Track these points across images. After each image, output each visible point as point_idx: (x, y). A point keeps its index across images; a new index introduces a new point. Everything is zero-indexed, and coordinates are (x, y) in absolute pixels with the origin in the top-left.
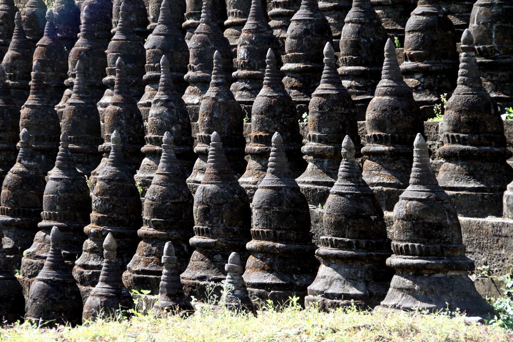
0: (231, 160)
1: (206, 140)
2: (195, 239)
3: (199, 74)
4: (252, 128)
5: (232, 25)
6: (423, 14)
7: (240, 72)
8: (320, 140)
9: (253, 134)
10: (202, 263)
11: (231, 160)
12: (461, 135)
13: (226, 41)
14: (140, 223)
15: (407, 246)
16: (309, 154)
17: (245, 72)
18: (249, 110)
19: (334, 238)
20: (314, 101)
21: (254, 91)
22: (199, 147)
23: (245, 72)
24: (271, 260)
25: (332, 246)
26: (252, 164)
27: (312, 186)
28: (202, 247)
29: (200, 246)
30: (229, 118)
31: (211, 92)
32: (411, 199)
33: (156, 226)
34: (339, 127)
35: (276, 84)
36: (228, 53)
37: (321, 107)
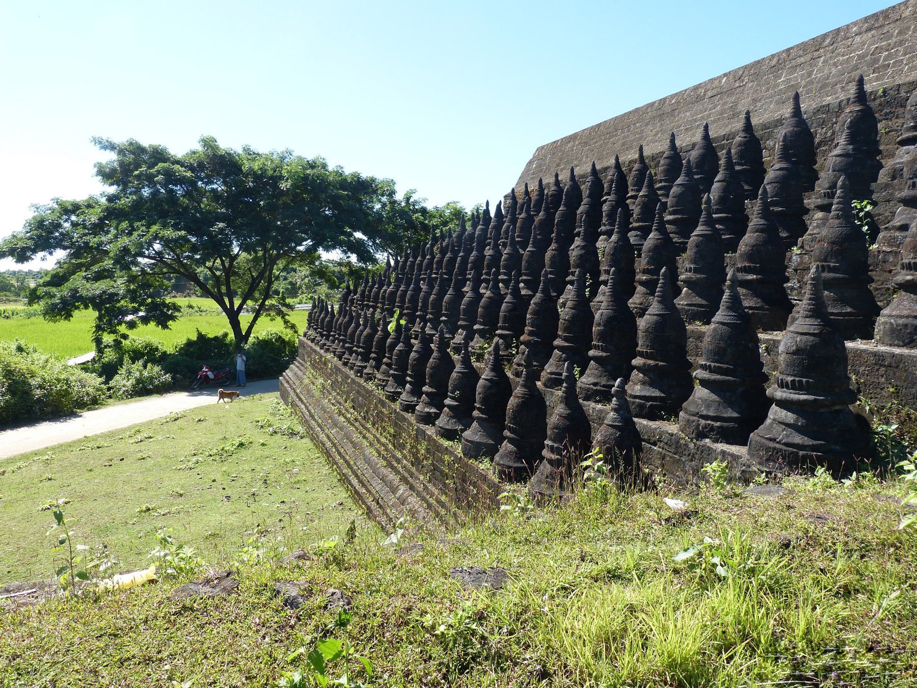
0: (623, 288)
1: (607, 272)
2: (591, 353)
3: (608, 228)
4: (642, 263)
5: (631, 197)
6: (780, 169)
7: (635, 225)
8: (696, 271)
9: (642, 267)
10: (596, 372)
11: (623, 288)
12: (832, 265)
13: (627, 205)
14: (556, 336)
15: (793, 381)
16: (684, 281)
17: (638, 224)
18: (640, 250)
19: (713, 364)
20: (693, 239)
21: (644, 236)
22: (603, 278)
23: (638, 224)
24: (653, 376)
25: (710, 372)
26: (640, 289)
27: (784, 448)
28: (596, 359)
29: (595, 358)
30: (624, 255)
31: (614, 237)
32: (802, 334)
33: (566, 339)
34: (862, 226)
35: (661, 229)
36: (628, 213)
37: (697, 246)
